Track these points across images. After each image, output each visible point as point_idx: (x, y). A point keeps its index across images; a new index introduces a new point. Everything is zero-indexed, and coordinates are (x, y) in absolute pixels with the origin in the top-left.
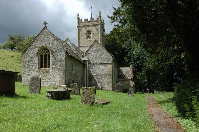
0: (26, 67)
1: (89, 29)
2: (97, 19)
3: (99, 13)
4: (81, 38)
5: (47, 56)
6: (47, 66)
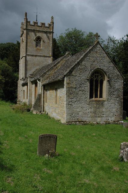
0: (72, 96)
1: (39, 34)
2: (50, 25)
3: (51, 18)
5: (99, 82)
6: (99, 97)
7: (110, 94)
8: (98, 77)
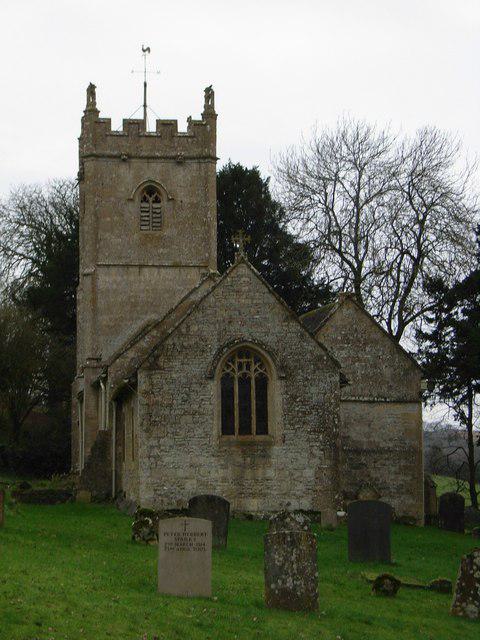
7: (293, 420)
8: (248, 367)
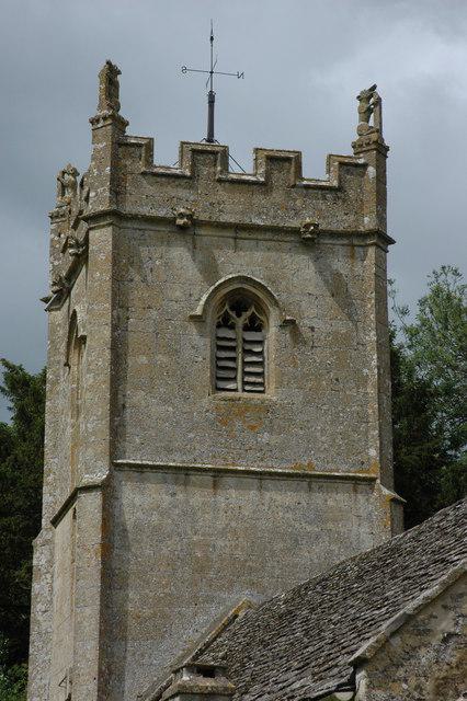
2: (346, 167)
3: (95, 87)
4: (137, 361)
